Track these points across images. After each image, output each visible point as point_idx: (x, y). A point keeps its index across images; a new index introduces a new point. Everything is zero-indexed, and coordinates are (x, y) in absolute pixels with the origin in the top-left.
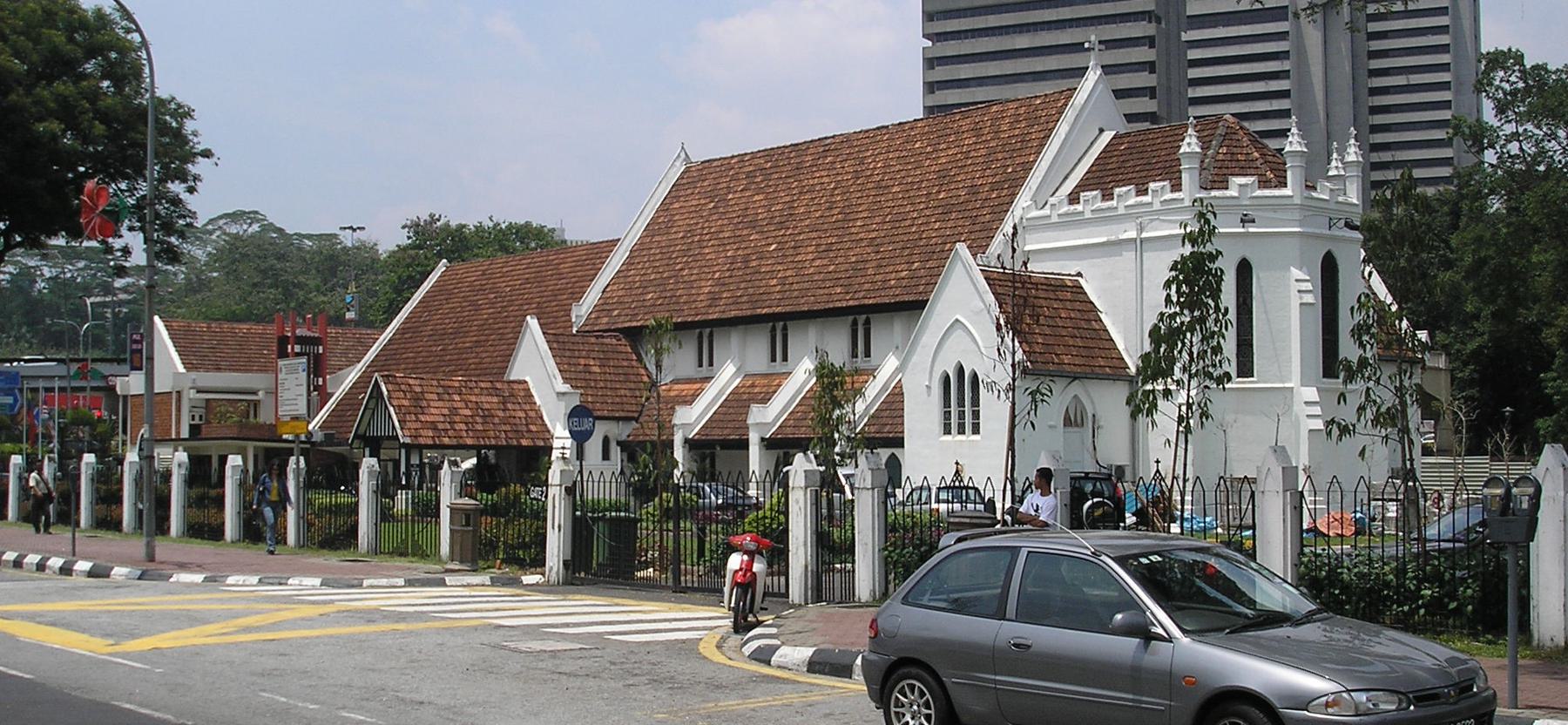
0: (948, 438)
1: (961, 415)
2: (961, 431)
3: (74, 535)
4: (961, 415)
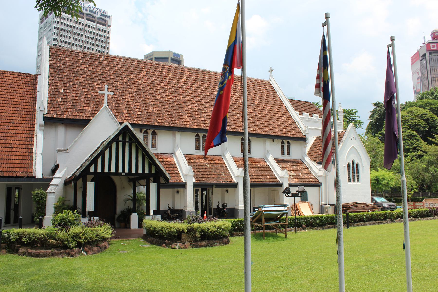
0: (349, 183)
1: (354, 176)
2: (354, 181)
3: (295, 216)
4: (354, 176)
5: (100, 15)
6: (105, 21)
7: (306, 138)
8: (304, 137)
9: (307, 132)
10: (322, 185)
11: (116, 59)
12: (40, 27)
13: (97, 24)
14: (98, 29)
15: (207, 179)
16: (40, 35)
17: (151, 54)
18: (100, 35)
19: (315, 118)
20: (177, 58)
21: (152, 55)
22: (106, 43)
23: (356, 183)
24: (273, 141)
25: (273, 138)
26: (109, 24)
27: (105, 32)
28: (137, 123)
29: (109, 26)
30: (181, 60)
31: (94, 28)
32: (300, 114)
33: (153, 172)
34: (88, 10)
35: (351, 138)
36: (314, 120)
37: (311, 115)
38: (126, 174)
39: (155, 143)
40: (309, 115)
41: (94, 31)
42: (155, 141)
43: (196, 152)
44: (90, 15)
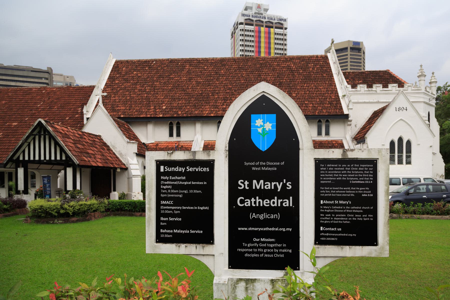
2: (400, 162)
5: (277, 20)
6: (282, 24)
11: (165, 62)
12: (231, 42)
20: (357, 47)
26: (285, 26)
27: (282, 34)
28: (158, 116)
29: (286, 29)
30: (361, 47)
33: (64, 158)
34: (267, 18)
35: (397, 109)
38: (47, 160)
40: (351, 87)
44: (269, 22)
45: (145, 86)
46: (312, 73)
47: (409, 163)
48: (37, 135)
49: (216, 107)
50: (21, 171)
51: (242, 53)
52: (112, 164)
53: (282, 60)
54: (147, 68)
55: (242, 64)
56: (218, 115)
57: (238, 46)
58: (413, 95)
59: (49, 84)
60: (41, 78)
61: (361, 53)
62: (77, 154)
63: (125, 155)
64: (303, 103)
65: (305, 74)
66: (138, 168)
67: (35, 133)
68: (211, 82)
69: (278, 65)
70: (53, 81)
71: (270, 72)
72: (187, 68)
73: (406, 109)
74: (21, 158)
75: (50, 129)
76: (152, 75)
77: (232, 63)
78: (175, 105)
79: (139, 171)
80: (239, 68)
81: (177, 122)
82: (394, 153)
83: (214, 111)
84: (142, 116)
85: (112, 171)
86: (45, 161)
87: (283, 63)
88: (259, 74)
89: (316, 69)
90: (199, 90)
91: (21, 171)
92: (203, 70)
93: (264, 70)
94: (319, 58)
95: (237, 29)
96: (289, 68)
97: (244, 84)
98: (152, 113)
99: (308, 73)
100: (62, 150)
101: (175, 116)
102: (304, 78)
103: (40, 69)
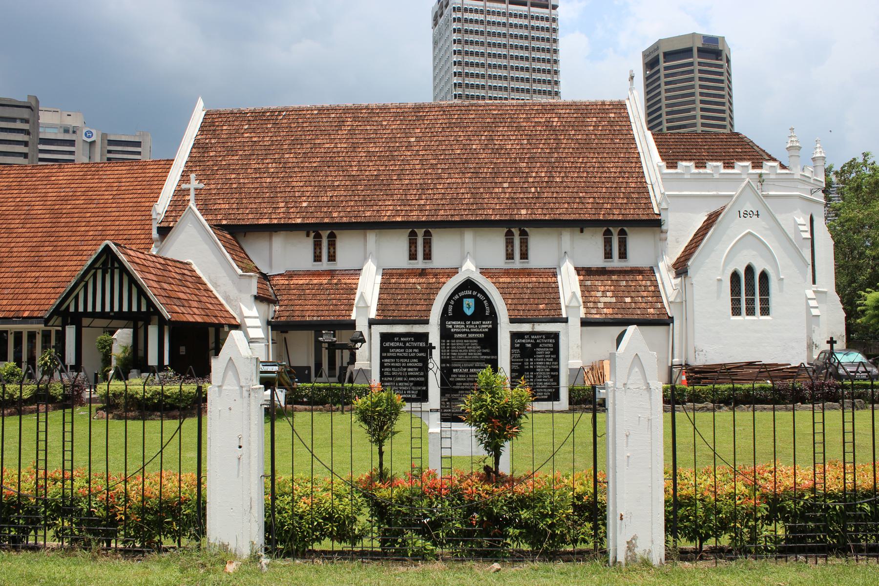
2: (751, 312)
7: (660, 220)
8: (656, 217)
9: (664, 206)
10: (673, 323)
11: (304, 112)
12: (434, 34)
13: (531, 8)
14: (532, 17)
15: (404, 313)
16: (434, 48)
17: (656, 47)
18: (538, 28)
19: (711, 172)
20: (712, 46)
21: (657, 49)
22: (551, 41)
23: (758, 317)
24: (582, 231)
25: (581, 225)
27: (547, 19)
29: (555, 7)
30: (720, 48)
31: (526, 17)
32: (698, 165)
33: (144, 309)
35: (742, 214)
36: (708, 177)
37: (701, 165)
38: (116, 313)
39: (334, 252)
41: (525, 22)
42: (334, 248)
43: (410, 263)
45: (267, 161)
46: (593, 137)
47: (765, 311)
48: (99, 268)
49: (405, 202)
50: (70, 332)
51: (457, 80)
52: (216, 317)
53: (536, 108)
54: (269, 126)
55: (456, 116)
56: (410, 219)
57: (448, 43)
58: (781, 184)
59: (31, 131)
60: (14, 120)
61: (721, 60)
62: (165, 302)
63: (236, 300)
64: (575, 195)
65: (580, 137)
66: (259, 324)
67: (97, 266)
68: (396, 154)
69: (527, 119)
70: (38, 123)
71: (512, 133)
72: (348, 123)
73: (758, 215)
74: (72, 309)
75: (123, 257)
76: (279, 138)
77: (437, 113)
78: (326, 200)
79: (260, 330)
80: (451, 126)
81: (329, 232)
82: (739, 294)
83: (402, 210)
84: (262, 222)
85: (212, 331)
86: (112, 314)
87: (537, 115)
88: (491, 138)
89: (600, 128)
90: (372, 170)
91: (70, 332)
92: (379, 127)
93: (501, 129)
94: (607, 107)
95: (446, 7)
96: (548, 125)
97: (462, 156)
98: (282, 215)
99: (585, 137)
100: (142, 293)
101: (326, 220)
102: (577, 146)
103: (11, 100)
